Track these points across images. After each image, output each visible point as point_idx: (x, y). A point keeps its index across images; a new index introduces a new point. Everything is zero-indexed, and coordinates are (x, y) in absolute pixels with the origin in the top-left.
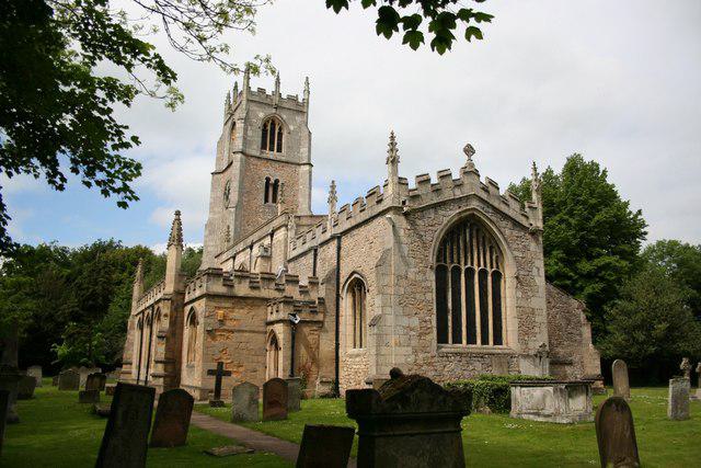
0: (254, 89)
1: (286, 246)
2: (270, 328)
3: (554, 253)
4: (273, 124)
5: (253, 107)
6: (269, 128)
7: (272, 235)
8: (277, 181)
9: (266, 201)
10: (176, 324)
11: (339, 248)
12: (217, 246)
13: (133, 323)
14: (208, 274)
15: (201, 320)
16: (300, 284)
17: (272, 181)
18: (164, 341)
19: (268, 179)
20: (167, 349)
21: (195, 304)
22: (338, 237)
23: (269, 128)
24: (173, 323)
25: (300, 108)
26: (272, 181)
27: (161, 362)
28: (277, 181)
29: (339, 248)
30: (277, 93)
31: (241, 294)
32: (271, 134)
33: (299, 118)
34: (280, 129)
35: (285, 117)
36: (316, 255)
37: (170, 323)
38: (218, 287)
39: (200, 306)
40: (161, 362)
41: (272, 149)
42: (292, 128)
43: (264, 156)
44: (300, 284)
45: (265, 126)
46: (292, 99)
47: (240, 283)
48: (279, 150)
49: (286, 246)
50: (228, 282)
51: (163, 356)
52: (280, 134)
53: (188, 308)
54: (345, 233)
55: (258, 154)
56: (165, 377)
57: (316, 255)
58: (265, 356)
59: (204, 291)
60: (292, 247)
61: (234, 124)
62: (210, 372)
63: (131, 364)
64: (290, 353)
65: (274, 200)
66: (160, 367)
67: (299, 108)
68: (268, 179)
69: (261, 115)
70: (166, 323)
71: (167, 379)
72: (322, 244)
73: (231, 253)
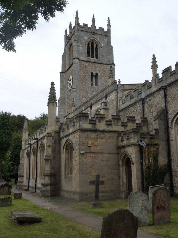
0: (81, 24)
1: (117, 103)
2: (122, 151)
3: (154, 132)
4: (93, 43)
5: (82, 34)
6: (90, 45)
7: (106, 97)
8: (97, 74)
9: (92, 85)
10: (56, 152)
11: (166, 95)
12: (65, 111)
13: (23, 154)
14: (80, 116)
15: (76, 147)
16: (137, 122)
17: (94, 74)
18: (49, 163)
19: (92, 73)
20: (51, 168)
21: (70, 137)
22: (165, 89)
23: (90, 45)
24: (54, 151)
25: (106, 34)
26: (94, 74)
27: (47, 176)
28: (97, 74)
29: (166, 95)
30: (93, 25)
31: (101, 129)
32: (93, 49)
33: (106, 40)
34: (97, 46)
35: (98, 39)
36: (143, 104)
37: (52, 151)
38: (86, 125)
39: (75, 139)
40: (47, 176)
41: (93, 57)
42: (103, 45)
43: (89, 60)
44: (137, 122)
45: (88, 44)
46: (101, 29)
47: (100, 122)
48: (97, 57)
49: (117, 103)
50: (93, 122)
51: (49, 172)
52: (97, 49)
53: (64, 141)
54: (170, 85)
55: (86, 60)
56: (51, 185)
57: (143, 104)
58: (119, 169)
59: (77, 127)
60: (121, 103)
61: (71, 45)
62: (92, 183)
63: (23, 177)
64: (140, 167)
65: (96, 84)
66: (47, 179)
67: (107, 34)
68: (92, 73)
69: (86, 38)
70: (49, 151)
71: (52, 186)
72: (148, 96)
73: (89, 105)
